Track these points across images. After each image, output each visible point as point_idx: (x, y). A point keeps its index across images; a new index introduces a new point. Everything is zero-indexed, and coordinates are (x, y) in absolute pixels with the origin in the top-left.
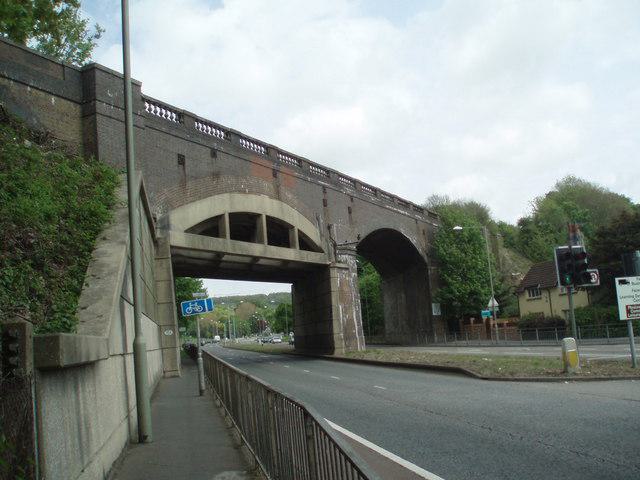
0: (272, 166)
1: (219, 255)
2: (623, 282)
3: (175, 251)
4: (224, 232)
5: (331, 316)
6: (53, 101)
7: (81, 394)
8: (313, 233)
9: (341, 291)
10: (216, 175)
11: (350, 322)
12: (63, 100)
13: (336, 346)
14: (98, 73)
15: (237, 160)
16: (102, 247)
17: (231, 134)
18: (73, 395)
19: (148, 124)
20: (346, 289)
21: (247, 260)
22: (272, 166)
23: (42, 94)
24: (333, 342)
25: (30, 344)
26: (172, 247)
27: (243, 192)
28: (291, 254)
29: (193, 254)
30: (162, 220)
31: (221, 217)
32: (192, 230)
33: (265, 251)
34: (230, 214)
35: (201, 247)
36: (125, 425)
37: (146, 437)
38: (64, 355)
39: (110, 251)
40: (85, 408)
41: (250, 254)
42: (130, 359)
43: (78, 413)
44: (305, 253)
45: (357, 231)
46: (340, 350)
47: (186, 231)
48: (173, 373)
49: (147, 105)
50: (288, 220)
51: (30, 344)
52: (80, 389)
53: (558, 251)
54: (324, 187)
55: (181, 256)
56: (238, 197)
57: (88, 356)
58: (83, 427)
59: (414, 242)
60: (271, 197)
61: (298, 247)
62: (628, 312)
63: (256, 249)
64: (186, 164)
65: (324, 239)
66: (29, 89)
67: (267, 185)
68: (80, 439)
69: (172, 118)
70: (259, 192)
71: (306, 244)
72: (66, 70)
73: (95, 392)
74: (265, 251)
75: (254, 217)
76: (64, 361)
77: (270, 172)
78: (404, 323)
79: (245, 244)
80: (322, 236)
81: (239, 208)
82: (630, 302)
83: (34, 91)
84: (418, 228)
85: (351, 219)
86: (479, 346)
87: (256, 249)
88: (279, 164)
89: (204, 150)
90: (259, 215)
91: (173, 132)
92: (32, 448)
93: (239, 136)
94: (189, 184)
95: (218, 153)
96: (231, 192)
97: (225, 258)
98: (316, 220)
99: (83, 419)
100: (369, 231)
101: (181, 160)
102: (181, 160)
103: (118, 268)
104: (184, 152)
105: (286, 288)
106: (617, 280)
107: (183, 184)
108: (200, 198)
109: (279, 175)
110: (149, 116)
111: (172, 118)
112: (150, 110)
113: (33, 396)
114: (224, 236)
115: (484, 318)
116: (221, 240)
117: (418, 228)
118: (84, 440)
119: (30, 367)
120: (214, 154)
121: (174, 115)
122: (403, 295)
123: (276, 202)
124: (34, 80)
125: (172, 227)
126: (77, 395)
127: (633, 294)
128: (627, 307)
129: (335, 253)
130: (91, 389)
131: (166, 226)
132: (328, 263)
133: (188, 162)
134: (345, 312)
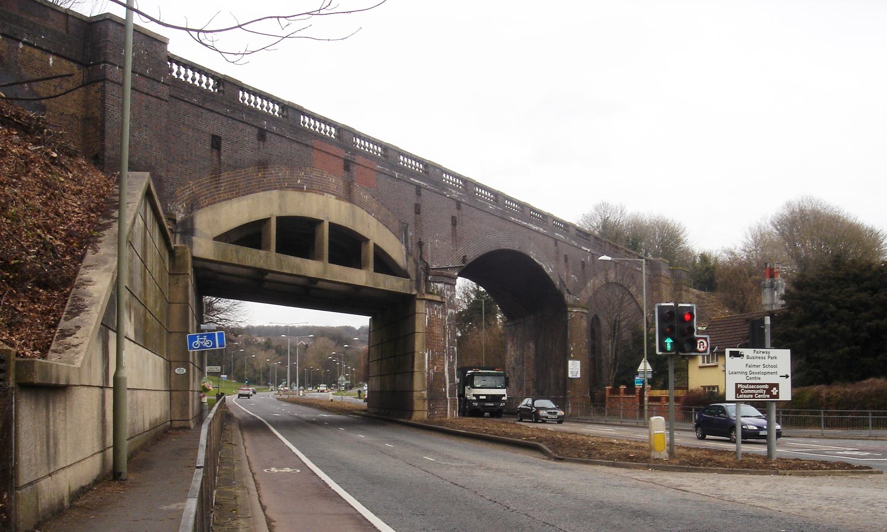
0: (343, 154)
1: (262, 272)
2: (735, 354)
3: (200, 264)
4: (270, 244)
5: (413, 367)
6: (51, 62)
7: (51, 413)
8: (396, 250)
9: (429, 332)
10: (263, 165)
11: (439, 377)
12: (64, 61)
13: (416, 408)
14: (111, 26)
15: (295, 146)
16: (85, 274)
17: (291, 111)
18: (44, 411)
19: (174, 93)
20: (437, 331)
21: (300, 281)
22: (343, 154)
23: (37, 53)
24: (412, 401)
25: (13, 365)
26: (194, 259)
27: (299, 189)
28: (360, 277)
29: (224, 268)
30: (184, 222)
31: (265, 221)
32: (225, 237)
33: (325, 272)
34: (280, 219)
35: (235, 261)
36: (98, 458)
37: (120, 474)
38: (38, 375)
39: (94, 279)
40: (54, 426)
41: (303, 274)
42: (110, 393)
43: (48, 427)
44: (381, 277)
45: (461, 252)
46: (421, 413)
47: (215, 239)
48: (183, 424)
49: (175, 67)
50: (360, 229)
51: (13, 365)
52: (51, 407)
53: (660, 308)
54: (418, 188)
55: (210, 270)
56: (292, 196)
57: (58, 379)
58: (52, 441)
59: (549, 271)
60: (339, 198)
61: (372, 269)
62: (738, 391)
63: (312, 268)
64: (222, 149)
65: (411, 259)
66: (21, 46)
67: (335, 181)
68: (48, 447)
69: (208, 85)
70: (322, 191)
71: (383, 263)
72: (70, 19)
73: (65, 414)
74: (325, 272)
75: (313, 224)
76: (37, 379)
77: (341, 163)
78: (531, 385)
79: (296, 260)
80: (409, 254)
81: (292, 211)
82: (742, 379)
83: (28, 49)
84: (557, 253)
85: (454, 233)
86: (606, 424)
87: (312, 268)
88: (356, 152)
89: (249, 129)
90: (320, 222)
91: (208, 105)
92: (11, 439)
93: (300, 111)
94: (225, 175)
95: (268, 135)
96: (281, 189)
97: (269, 276)
98: (402, 233)
99: (51, 433)
100: (480, 252)
101: (216, 142)
102: (216, 142)
103: (100, 297)
104: (222, 132)
105: (360, 322)
106: (728, 351)
107: (216, 174)
108: (238, 195)
109: (354, 168)
110: (177, 83)
111: (208, 85)
112: (179, 74)
113: (14, 402)
114: (267, 248)
115: (638, 385)
116: (262, 253)
117: (557, 253)
118: (52, 451)
119: (12, 384)
120: (262, 135)
121: (211, 81)
122: (532, 345)
123: (345, 205)
124: (29, 34)
125: (197, 233)
126: (48, 412)
127: (748, 370)
128: (737, 384)
129: (426, 279)
130: (62, 412)
131: (187, 230)
132: (414, 293)
133: (224, 145)
134: (432, 362)
